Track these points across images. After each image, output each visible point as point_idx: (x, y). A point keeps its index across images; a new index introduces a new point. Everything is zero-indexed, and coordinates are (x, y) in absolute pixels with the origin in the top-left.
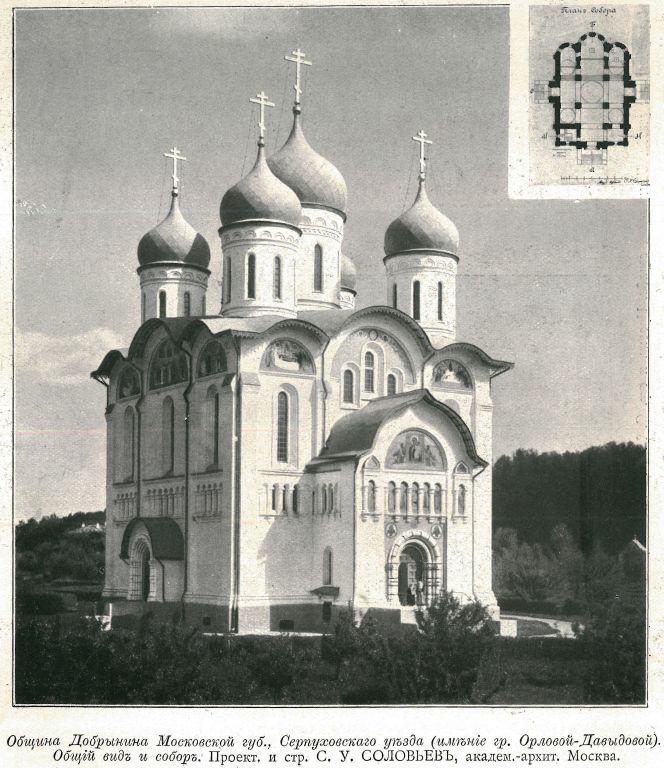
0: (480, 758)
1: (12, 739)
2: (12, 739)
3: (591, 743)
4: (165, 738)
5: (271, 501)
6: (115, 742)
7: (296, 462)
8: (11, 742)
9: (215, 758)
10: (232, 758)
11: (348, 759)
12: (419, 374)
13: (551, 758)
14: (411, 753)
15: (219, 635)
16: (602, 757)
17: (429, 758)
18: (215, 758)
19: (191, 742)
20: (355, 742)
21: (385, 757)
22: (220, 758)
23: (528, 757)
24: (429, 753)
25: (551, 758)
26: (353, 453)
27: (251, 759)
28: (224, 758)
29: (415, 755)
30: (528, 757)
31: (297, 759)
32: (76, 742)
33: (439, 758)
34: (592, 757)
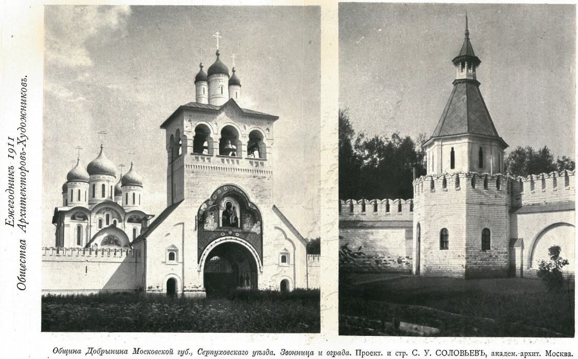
0: (499, 354)
1: (56, 349)
2: (56, 349)
3: (92, 352)
4: (137, 349)
5: (110, 190)
6: (110, 352)
7: (82, 246)
8: (55, 351)
9: (358, 353)
10: (368, 354)
11: (429, 354)
12: (365, 223)
13: (536, 354)
14: (462, 352)
15: (357, 317)
16: (564, 354)
17: (472, 354)
18: (358, 353)
19: (150, 352)
20: (237, 353)
21: (448, 353)
22: (361, 354)
23: (524, 354)
24: (472, 352)
25: (536, 354)
26: (250, 283)
27: (378, 354)
28: (526, 354)
29: (464, 353)
30: (524, 354)
31: (402, 354)
32: (90, 352)
33: (477, 354)
34: (558, 354)
